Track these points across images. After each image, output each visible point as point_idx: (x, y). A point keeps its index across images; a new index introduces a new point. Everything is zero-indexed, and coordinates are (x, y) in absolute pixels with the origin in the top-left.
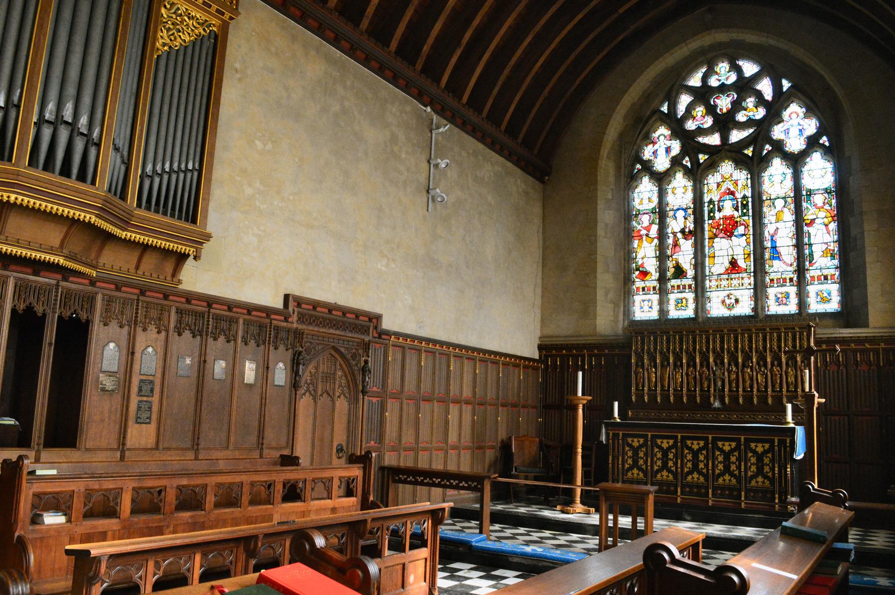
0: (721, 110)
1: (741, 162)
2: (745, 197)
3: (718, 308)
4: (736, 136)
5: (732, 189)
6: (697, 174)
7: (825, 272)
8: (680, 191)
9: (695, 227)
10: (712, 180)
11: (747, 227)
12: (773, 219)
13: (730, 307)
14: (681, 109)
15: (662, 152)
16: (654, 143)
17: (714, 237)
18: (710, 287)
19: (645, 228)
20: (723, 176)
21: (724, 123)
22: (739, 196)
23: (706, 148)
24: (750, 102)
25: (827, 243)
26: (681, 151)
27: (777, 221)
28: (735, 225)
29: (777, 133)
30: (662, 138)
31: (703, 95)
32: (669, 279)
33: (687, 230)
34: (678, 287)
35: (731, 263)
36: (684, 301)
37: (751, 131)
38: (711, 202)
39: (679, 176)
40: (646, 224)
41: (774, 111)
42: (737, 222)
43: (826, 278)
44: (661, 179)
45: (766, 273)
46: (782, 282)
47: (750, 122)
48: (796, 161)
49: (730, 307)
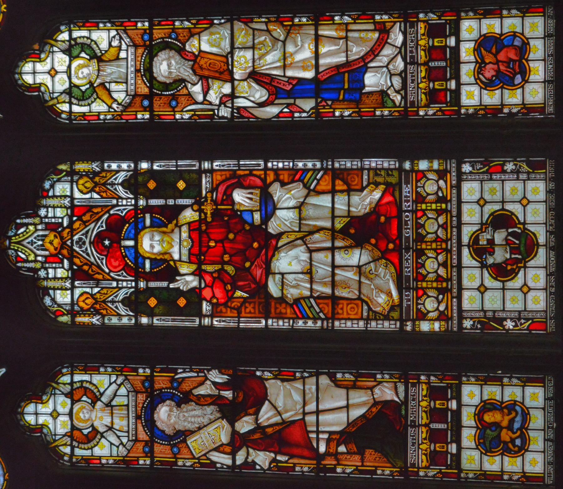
2: (134, 184)
5: (101, 226)
11: (237, 180)
12: (219, 90)
13: (524, 246)
20: (54, 259)
22: (126, 202)
26: (157, 406)
32: (404, 471)
34: (435, 436)
35: (359, 242)
36: (488, 418)
38: (135, 303)
42: (216, 213)
45: (405, 113)
46: (427, 284)
49: (524, 246)
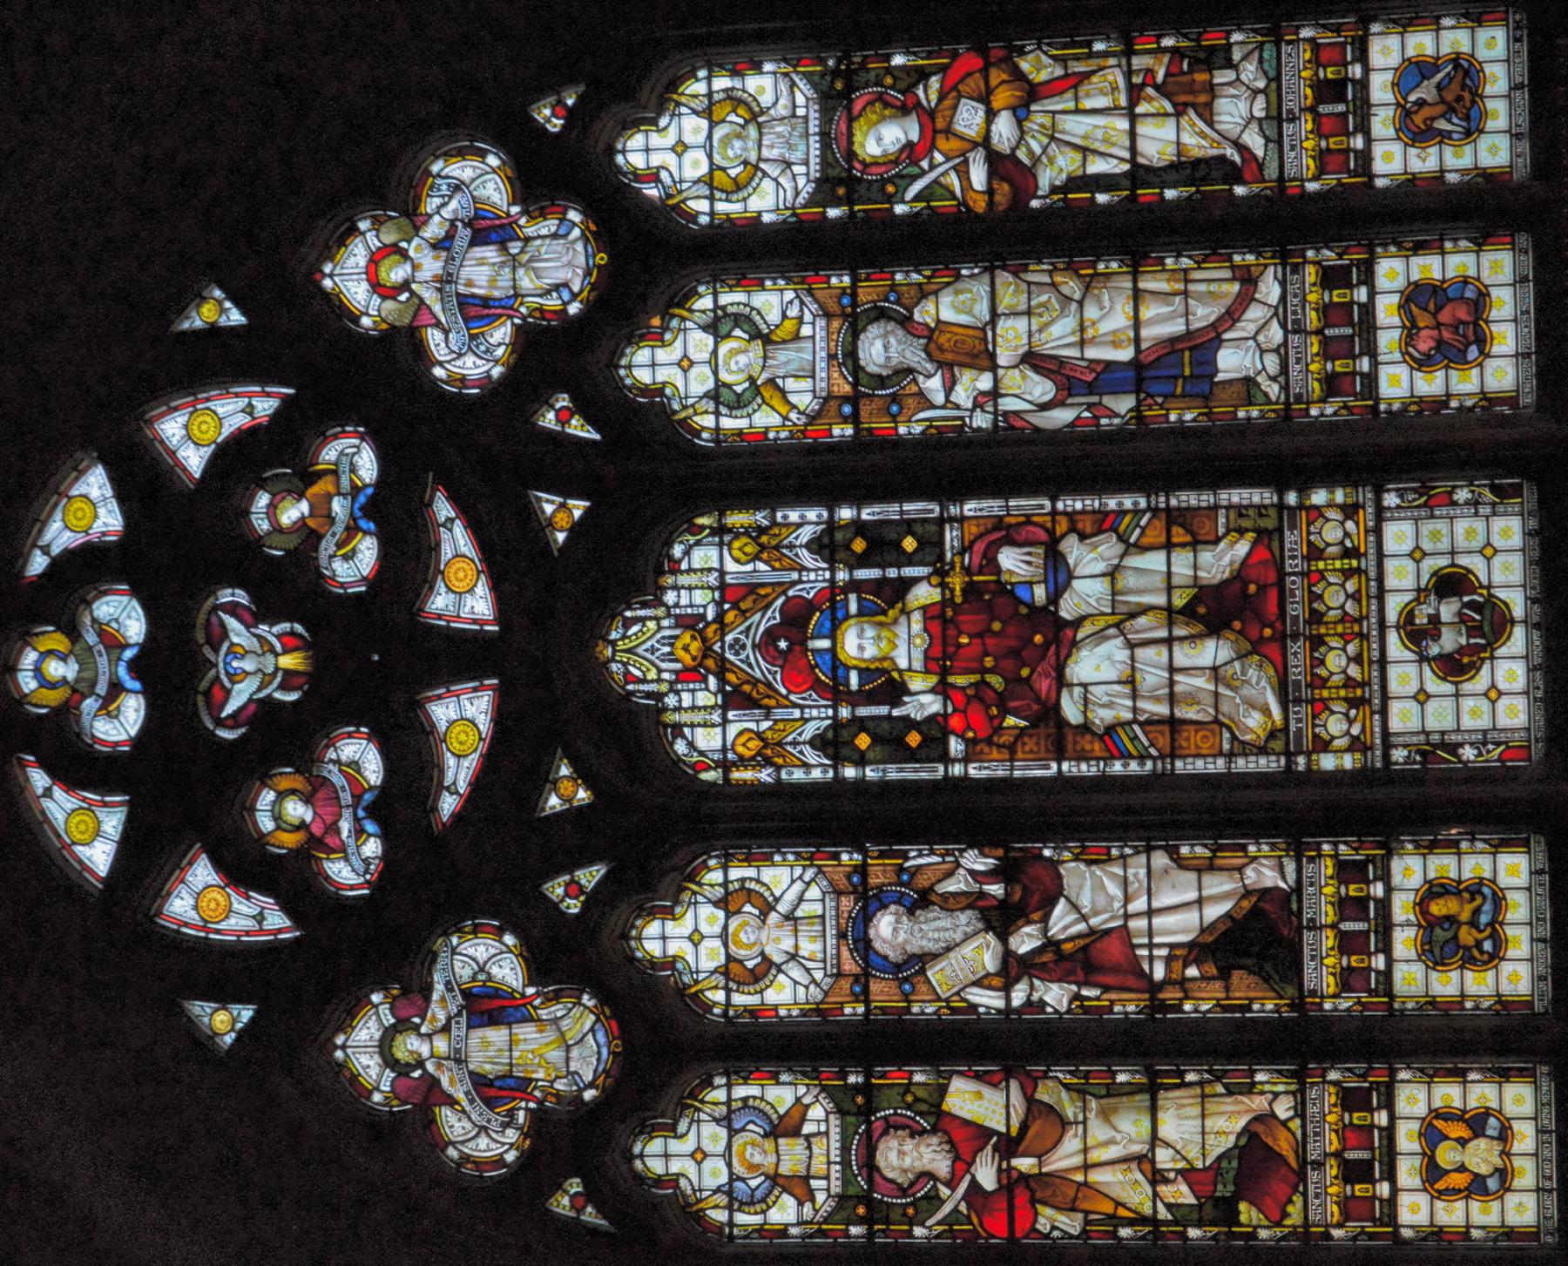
0: (289, 679)
1: (622, 567)
2: (828, 546)
3: (1493, 694)
4: (464, 598)
6: (670, 825)
7: (1298, 92)
8: (751, 933)
9: (978, 842)
10: (707, 735)
11: (1005, 533)
13: (1489, 623)
14: (250, 917)
15: (489, 1047)
16: (432, 1094)
17: (1056, 735)
18: (1356, 745)
19: (962, 1163)
20: (690, 675)
21: (373, 659)
22: (814, 576)
23: (512, 759)
24: (276, 513)
25: (1135, 94)
27: (988, 361)
28: (989, 596)
29: (466, 361)
30: (409, 1046)
31: (185, 788)
32: (1298, 1004)
33: (996, 889)
34: (1347, 943)
35: (1214, 627)
36: (1437, 908)
37: (443, 508)
38: (833, 744)
39: (658, 938)
40: (931, 1156)
41: (369, 376)
42: (970, 590)
43: (1329, 90)
44: (672, 1046)
45: (1287, 413)
47: (396, 515)
48: (655, 259)
49: (1489, 623)
